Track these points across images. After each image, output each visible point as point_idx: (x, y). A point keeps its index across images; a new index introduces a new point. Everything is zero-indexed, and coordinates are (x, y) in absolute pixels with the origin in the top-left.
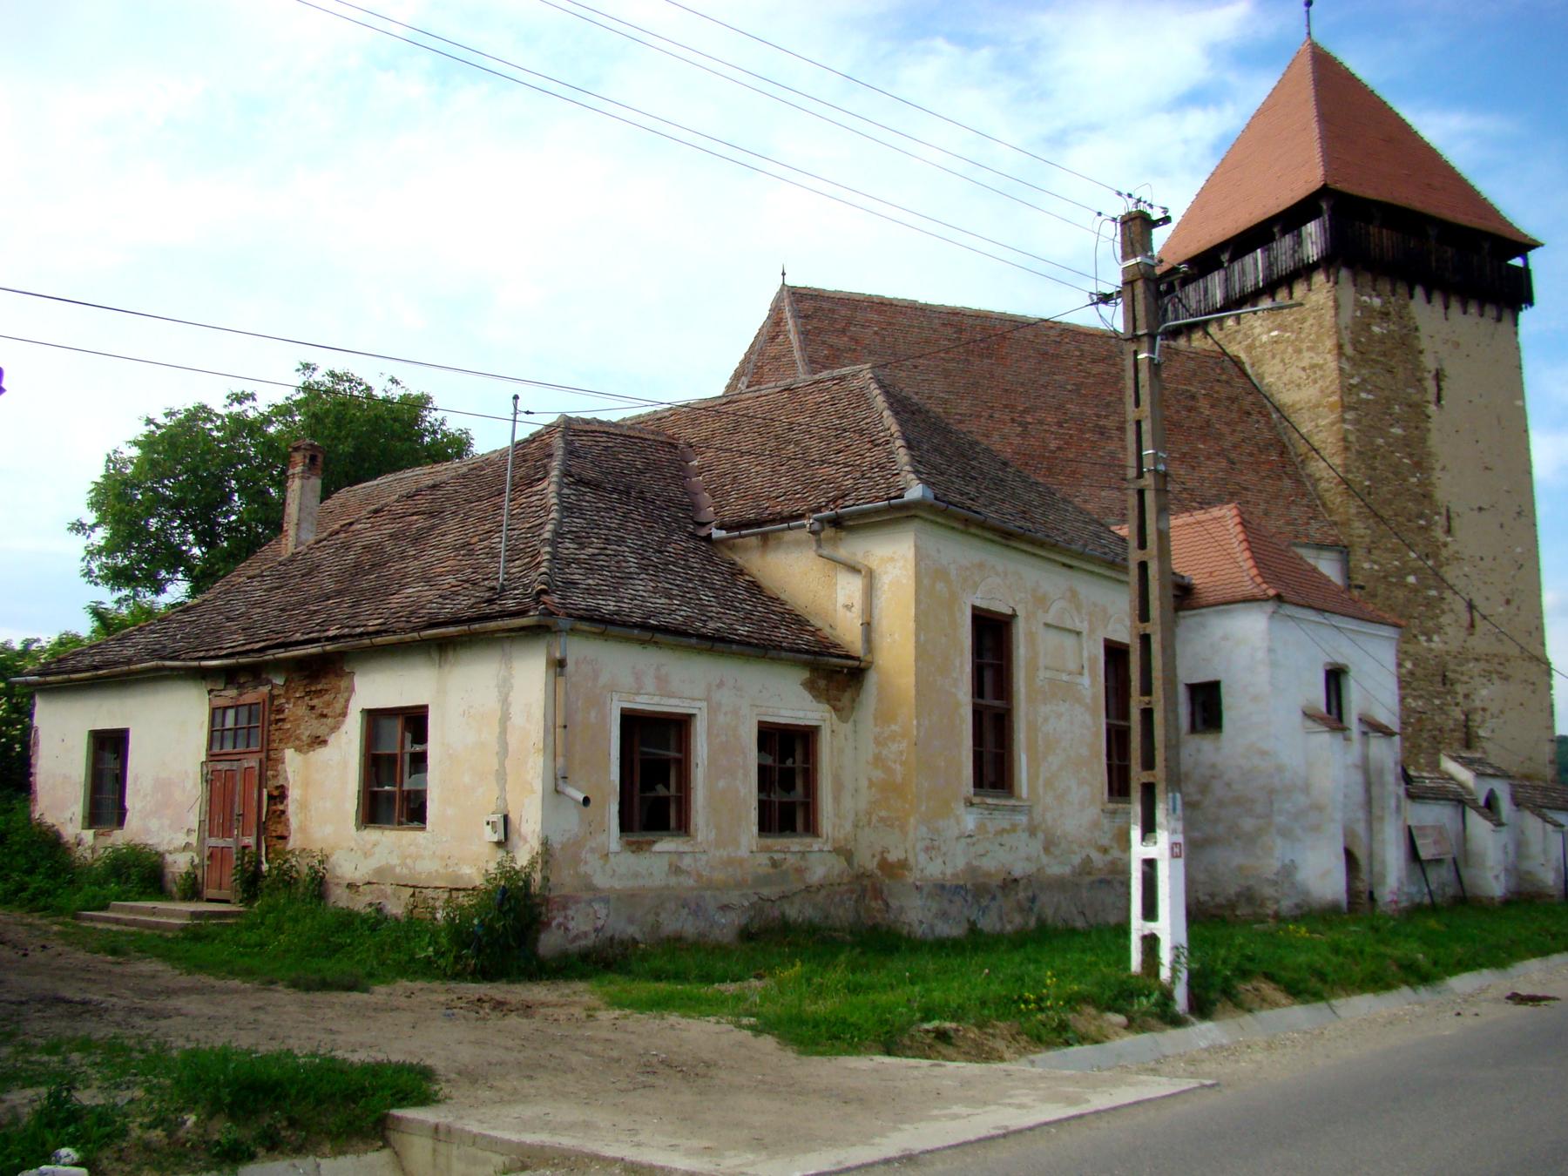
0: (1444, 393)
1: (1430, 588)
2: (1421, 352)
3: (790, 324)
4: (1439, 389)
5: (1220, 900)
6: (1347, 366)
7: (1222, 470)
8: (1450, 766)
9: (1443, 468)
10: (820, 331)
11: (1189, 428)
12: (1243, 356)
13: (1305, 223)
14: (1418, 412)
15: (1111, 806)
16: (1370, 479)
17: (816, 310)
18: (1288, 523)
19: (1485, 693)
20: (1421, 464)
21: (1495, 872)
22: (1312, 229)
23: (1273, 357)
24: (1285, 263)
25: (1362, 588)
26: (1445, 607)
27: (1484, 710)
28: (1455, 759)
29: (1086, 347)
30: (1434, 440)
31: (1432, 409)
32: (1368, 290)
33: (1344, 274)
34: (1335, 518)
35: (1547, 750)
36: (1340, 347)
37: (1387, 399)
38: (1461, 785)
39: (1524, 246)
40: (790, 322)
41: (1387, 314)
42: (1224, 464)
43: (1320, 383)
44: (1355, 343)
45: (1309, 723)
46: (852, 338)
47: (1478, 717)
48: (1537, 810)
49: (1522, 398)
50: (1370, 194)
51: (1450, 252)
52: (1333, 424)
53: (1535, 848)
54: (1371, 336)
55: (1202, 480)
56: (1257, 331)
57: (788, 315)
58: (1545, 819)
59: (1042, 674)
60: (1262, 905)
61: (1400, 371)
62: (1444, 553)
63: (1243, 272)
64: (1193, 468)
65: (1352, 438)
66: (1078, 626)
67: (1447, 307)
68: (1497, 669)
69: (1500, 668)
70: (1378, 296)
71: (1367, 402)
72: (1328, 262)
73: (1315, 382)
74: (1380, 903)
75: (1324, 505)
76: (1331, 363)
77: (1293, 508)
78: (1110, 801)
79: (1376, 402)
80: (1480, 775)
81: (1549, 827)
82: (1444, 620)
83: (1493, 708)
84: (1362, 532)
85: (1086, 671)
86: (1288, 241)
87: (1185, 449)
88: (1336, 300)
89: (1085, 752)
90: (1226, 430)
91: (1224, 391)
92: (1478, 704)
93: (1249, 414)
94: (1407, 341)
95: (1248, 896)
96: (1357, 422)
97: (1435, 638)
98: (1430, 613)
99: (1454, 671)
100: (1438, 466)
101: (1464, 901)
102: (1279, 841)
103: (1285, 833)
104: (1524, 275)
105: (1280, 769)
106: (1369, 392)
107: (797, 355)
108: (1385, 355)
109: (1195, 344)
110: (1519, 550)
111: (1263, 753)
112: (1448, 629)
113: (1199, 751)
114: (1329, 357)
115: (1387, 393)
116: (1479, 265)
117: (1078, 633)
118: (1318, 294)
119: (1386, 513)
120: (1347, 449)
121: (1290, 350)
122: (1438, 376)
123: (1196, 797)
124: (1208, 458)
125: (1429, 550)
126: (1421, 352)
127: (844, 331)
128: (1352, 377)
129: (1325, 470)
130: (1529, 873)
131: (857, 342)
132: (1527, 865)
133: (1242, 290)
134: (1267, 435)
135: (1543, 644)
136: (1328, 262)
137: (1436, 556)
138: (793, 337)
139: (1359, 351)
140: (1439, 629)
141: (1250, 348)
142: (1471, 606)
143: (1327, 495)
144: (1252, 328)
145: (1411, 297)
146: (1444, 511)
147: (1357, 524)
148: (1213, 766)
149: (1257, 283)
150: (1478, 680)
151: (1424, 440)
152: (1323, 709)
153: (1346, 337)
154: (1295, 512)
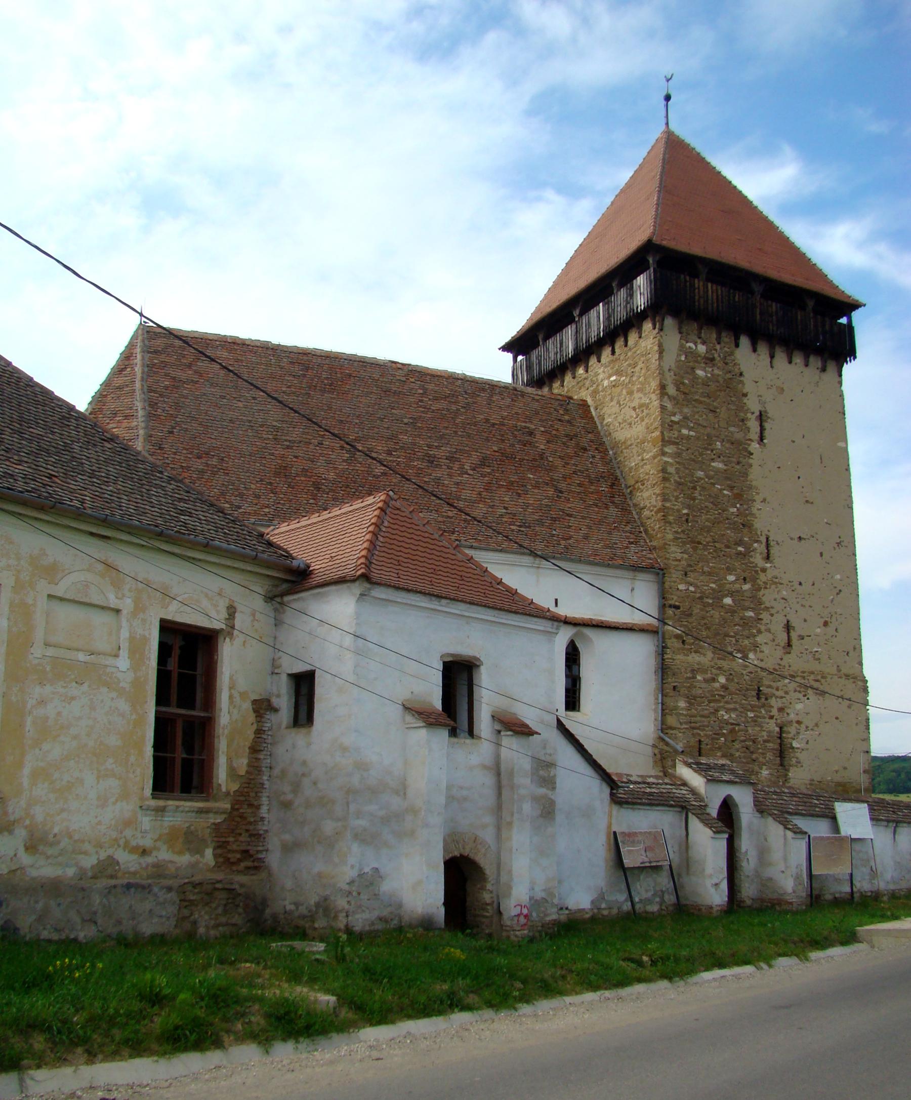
0: (766, 433)
1: (747, 609)
2: (745, 395)
3: (138, 360)
4: (762, 429)
5: (303, 910)
6: (669, 406)
7: (547, 497)
8: (685, 772)
9: (764, 500)
10: (164, 365)
11: (521, 460)
12: (590, 401)
13: (635, 278)
14: (741, 450)
15: (154, 803)
16: (689, 507)
17: (168, 346)
18: (607, 546)
19: (801, 707)
20: (742, 495)
21: (715, 881)
22: (641, 282)
23: (612, 400)
24: (620, 314)
25: (677, 607)
26: (763, 628)
27: (799, 722)
28: (689, 765)
29: (431, 387)
30: (755, 474)
31: (754, 446)
32: (695, 338)
33: (669, 322)
34: (654, 543)
35: (861, 763)
36: (663, 387)
37: (708, 435)
38: (693, 791)
39: (850, 306)
40: (139, 357)
41: (713, 359)
42: (551, 492)
43: (646, 420)
44: (678, 385)
45: (409, 718)
46: (196, 372)
47: (792, 730)
48: (783, 817)
49: (845, 440)
50: (697, 250)
51: (774, 307)
52: (654, 457)
53: (776, 855)
54: (696, 377)
55: (528, 505)
56: (601, 377)
57: (138, 350)
58: (785, 825)
59: (37, 651)
60: (336, 917)
61: (723, 413)
62: (762, 577)
63: (589, 325)
64: (519, 495)
65: (671, 470)
66: (113, 601)
67: (772, 357)
68: (812, 685)
69: (816, 685)
70: (704, 343)
71: (688, 438)
72: (657, 309)
73: (642, 420)
74: (505, 916)
75: (646, 531)
76: (655, 402)
77: (615, 533)
78: (154, 797)
79: (698, 438)
80: (711, 781)
81: (789, 834)
82: (759, 639)
83: (807, 721)
84: (679, 556)
85: (124, 653)
86: (623, 293)
87: (514, 478)
88: (660, 345)
89: (113, 741)
90: (559, 463)
91: (563, 429)
92: (792, 716)
93: (585, 449)
94: (732, 385)
95: (325, 907)
96: (678, 455)
97: (751, 655)
98: (746, 633)
99: (769, 687)
100: (758, 498)
101: (684, 912)
102: (355, 848)
103: (366, 838)
104: (849, 332)
105: (362, 766)
106: (690, 429)
107: (138, 385)
108: (709, 396)
109: (555, 391)
110: (838, 577)
111: (344, 749)
112: (764, 648)
113: (294, 746)
114: (654, 397)
115: (709, 430)
116: (812, 323)
117: (118, 611)
118: (645, 340)
119: (705, 539)
120: (665, 479)
121: (624, 392)
122: (762, 418)
123: (290, 796)
124: (535, 487)
125: (746, 574)
126: (745, 395)
127: (190, 366)
128: (674, 415)
129: (648, 497)
130: (771, 879)
131: (201, 375)
132: (770, 872)
133: (587, 341)
134: (601, 468)
135: (861, 664)
136: (657, 309)
137: (754, 580)
138: (138, 370)
139: (680, 391)
140: (755, 647)
141: (595, 392)
142: (788, 627)
143: (648, 522)
144: (597, 374)
145: (737, 346)
146: (763, 539)
147: (673, 549)
148: (304, 763)
149: (599, 334)
150: (793, 695)
151: (745, 475)
152: (438, 705)
153: (669, 378)
154: (616, 537)
